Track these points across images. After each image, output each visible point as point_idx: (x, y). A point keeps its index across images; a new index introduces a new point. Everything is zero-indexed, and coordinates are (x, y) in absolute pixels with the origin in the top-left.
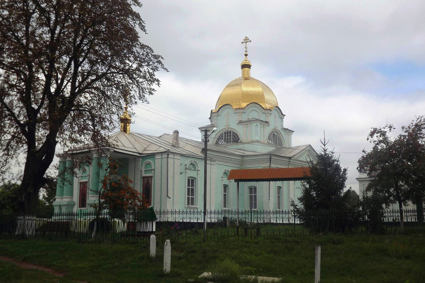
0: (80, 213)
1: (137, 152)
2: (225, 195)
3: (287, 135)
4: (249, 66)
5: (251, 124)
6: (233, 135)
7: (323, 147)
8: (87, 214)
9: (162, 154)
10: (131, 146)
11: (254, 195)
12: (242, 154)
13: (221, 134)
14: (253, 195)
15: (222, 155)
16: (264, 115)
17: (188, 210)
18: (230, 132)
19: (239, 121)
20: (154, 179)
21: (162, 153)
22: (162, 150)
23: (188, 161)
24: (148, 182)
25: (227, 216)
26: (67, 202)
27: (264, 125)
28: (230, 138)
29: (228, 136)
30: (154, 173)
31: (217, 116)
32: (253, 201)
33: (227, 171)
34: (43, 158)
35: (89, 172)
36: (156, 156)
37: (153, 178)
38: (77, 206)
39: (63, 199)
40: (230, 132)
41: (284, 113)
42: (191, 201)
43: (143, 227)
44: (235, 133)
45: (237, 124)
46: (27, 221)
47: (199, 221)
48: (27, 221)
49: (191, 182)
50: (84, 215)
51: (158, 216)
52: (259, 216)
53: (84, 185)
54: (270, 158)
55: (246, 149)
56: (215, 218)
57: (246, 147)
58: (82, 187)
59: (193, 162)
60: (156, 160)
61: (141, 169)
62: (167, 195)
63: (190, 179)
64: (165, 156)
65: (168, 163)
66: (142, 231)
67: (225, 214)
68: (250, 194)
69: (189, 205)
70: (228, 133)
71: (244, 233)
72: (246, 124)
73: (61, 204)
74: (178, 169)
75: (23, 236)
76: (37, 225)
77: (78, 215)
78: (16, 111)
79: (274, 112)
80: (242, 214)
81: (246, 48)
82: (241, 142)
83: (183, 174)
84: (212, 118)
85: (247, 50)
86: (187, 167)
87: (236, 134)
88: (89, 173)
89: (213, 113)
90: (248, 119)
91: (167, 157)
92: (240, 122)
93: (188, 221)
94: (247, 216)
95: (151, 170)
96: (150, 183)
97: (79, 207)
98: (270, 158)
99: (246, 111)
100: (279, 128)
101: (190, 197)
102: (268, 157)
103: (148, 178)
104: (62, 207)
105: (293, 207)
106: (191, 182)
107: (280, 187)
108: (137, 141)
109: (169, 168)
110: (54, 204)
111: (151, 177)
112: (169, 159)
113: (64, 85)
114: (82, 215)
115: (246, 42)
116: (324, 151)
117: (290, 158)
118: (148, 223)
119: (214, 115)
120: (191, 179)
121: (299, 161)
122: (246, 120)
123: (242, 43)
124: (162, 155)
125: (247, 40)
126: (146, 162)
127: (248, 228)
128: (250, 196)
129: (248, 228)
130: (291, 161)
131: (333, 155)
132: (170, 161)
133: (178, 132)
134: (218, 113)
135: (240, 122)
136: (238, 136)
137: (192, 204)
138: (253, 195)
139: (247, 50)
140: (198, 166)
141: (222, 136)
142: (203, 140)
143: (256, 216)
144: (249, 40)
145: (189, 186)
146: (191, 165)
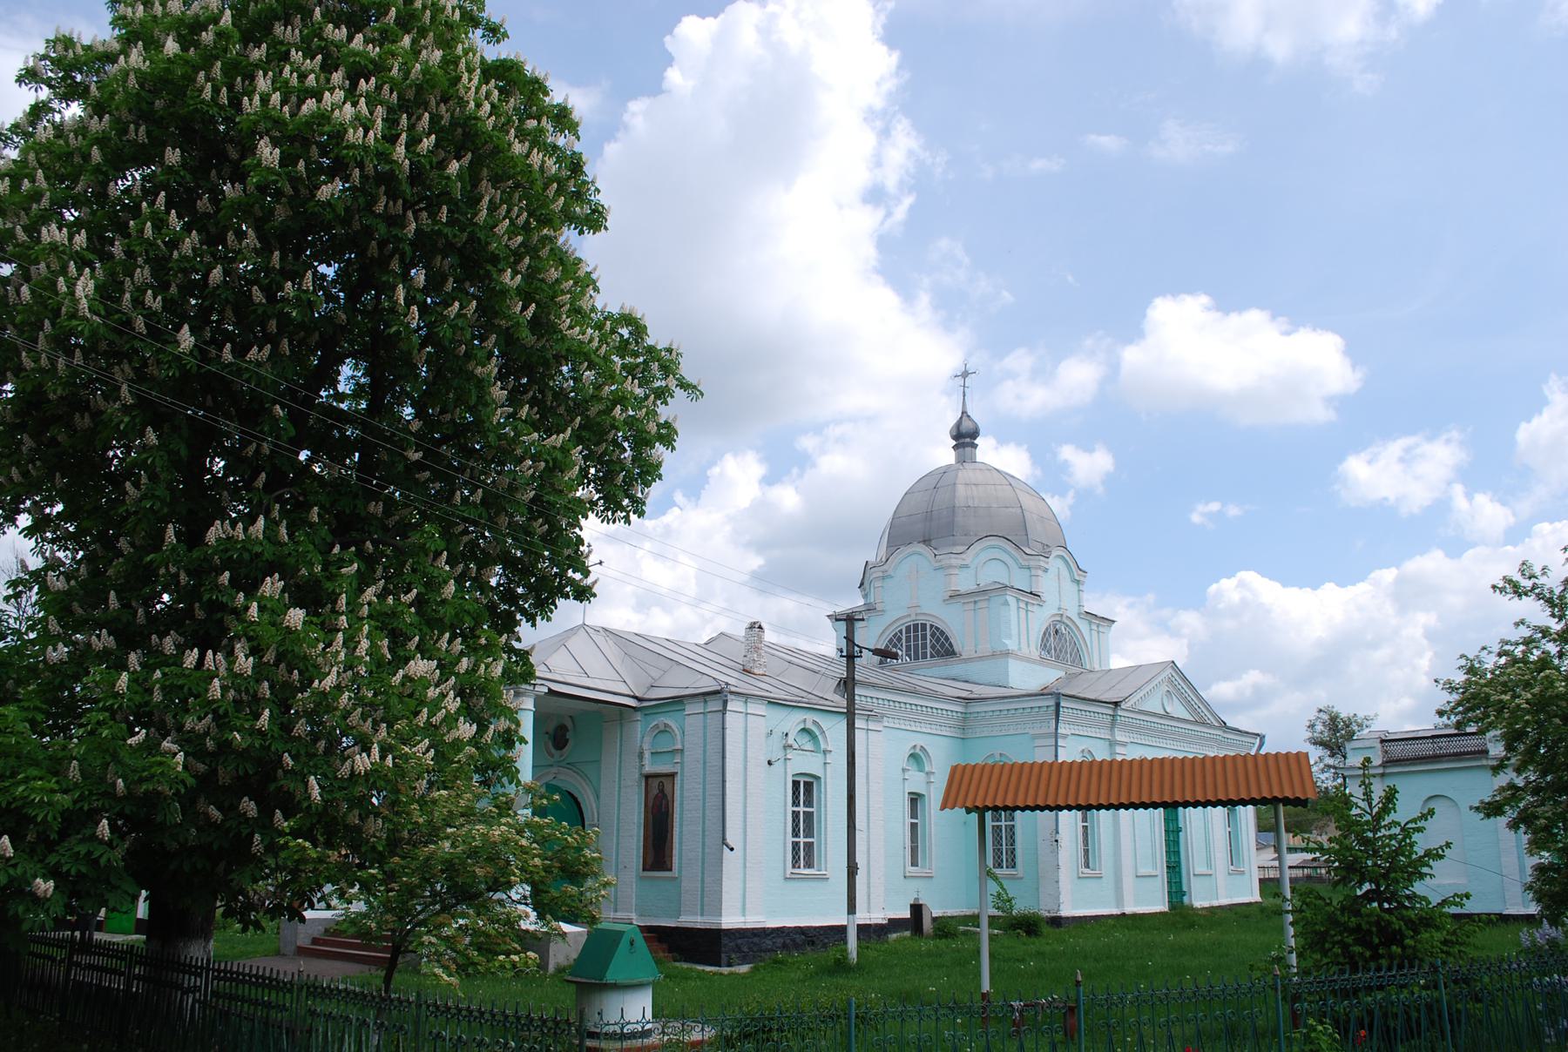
2: (914, 826)
3: (1095, 634)
6: (933, 635)
12: (964, 694)
18: (924, 626)
19: (949, 593)
20: (682, 780)
24: (662, 791)
28: (924, 645)
30: (682, 763)
33: (918, 751)
37: (678, 780)
40: (924, 626)
44: (937, 628)
49: (804, 789)
54: (1058, 705)
55: (974, 678)
59: (809, 725)
62: (724, 839)
64: (714, 705)
69: (799, 867)
70: (916, 630)
74: (760, 751)
83: (778, 766)
87: (942, 633)
92: (955, 596)
96: (669, 798)
100: (1072, 613)
102: (1052, 702)
106: (804, 789)
111: (672, 775)
117: (1116, 704)
120: (802, 780)
122: (973, 587)
124: (705, 702)
125: (965, 374)
128: (993, 826)
130: (1120, 713)
133: (760, 627)
136: (947, 639)
138: (802, 840)
145: (798, 805)
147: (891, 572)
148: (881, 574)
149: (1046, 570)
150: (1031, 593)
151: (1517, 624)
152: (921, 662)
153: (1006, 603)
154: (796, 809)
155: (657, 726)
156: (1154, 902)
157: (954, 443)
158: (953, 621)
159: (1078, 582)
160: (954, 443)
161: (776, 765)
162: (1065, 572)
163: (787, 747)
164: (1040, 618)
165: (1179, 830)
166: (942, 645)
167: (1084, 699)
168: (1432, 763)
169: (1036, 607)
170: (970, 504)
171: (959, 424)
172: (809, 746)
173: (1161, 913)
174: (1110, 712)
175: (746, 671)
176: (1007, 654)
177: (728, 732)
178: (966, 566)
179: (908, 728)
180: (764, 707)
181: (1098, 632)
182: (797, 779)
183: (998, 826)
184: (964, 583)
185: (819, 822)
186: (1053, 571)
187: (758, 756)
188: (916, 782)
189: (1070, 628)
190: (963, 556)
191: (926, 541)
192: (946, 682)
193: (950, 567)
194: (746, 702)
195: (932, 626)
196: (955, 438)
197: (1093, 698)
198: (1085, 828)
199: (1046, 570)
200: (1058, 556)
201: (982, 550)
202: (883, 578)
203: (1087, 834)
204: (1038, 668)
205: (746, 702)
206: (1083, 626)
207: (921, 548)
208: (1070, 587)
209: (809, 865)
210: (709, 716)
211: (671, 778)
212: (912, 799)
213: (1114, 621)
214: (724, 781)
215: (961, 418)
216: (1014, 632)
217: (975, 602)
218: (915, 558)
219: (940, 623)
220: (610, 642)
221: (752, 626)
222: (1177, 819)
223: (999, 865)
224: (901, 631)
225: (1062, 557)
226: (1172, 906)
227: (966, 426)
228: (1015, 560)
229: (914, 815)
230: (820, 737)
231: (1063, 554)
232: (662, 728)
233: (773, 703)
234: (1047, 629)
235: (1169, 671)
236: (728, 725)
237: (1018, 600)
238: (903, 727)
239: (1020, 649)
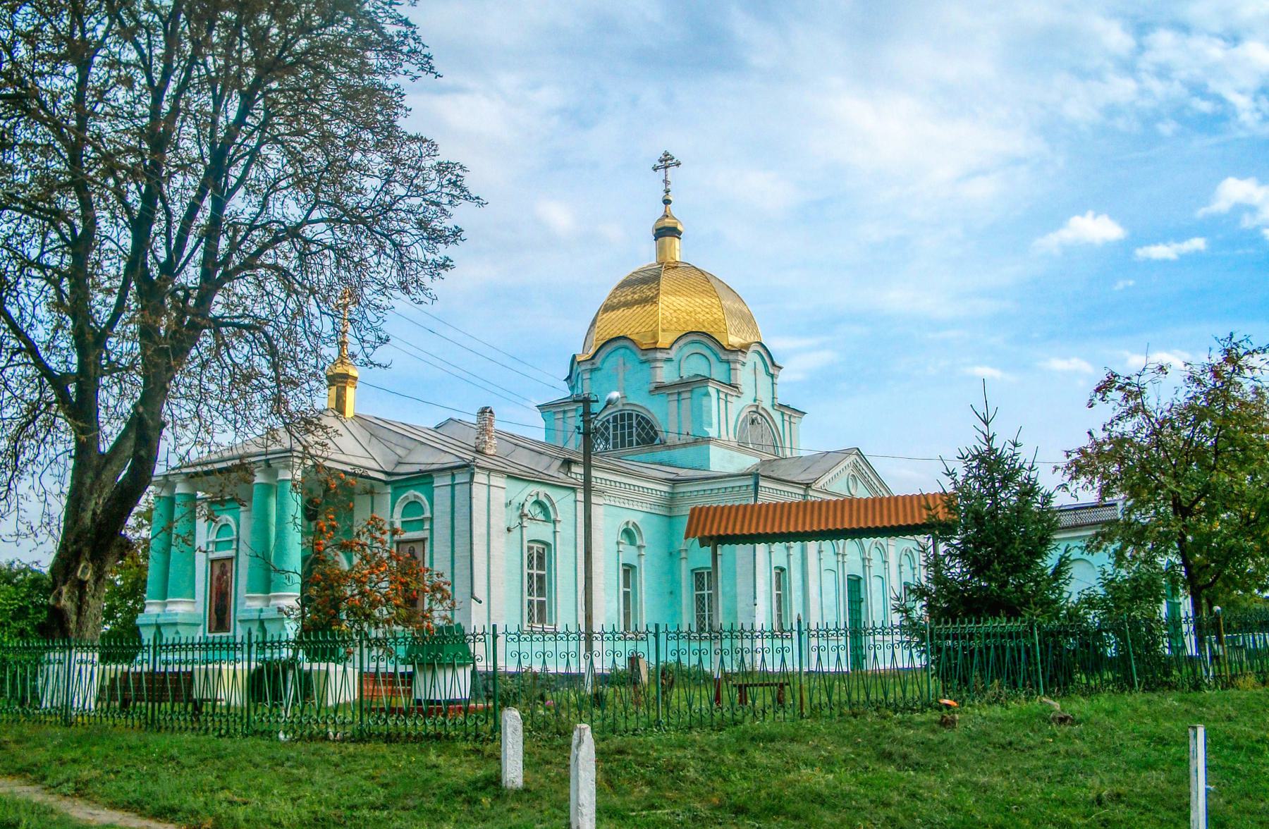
0: (246, 641)
1: (377, 467)
2: (626, 595)
4: (673, 232)
5: (691, 391)
6: (639, 424)
7: (983, 427)
9: (455, 472)
10: (361, 452)
12: (671, 477)
15: (618, 479)
18: (630, 416)
19: (654, 385)
20: (432, 545)
21: (452, 470)
22: (449, 460)
28: (630, 435)
29: (623, 427)
30: (431, 530)
31: (592, 371)
33: (630, 526)
35: (238, 526)
36: (435, 480)
38: (204, 629)
39: (165, 605)
40: (630, 416)
41: (777, 363)
42: (539, 611)
44: (643, 418)
45: (650, 392)
46: (78, 667)
48: (78, 667)
51: (479, 649)
53: (223, 566)
54: (756, 484)
55: (679, 463)
57: (678, 454)
58: (217, 572)
59: (542, 498)
60: (436, 491)
61: (392, 516)
62: (472, 593)
63: (532, 548)
64: (461, 478)
66: (458, 697)
70: (623, 419)
73: (161, 620)
74: (501, 519)
75: (64, 715)
77: (239, 646)
78: (40, 334)
79: (751, 358)
80: (772, 638)
81: (666, 182)
82: (663, 443)
83: (516, 532)
85: (669, 187)
86: (526, 511)
87: (648, 422)
88: (238, 532)
89: (579, 363)
92: (659, 388)
94: (787, 643)
95: (422, 521)
97: (210, 631)
100: (767, 404)
101: (535, 598)
102: (751, 482)
103: (412, 545)
105: (900, 614)
107: (782, 570)
108: (376, 437)
110: (141, 619)
111: (423, 540)
113: (186, 253)
114: (255, 646)
115: (666, 167)
116: (984, 441)
117: (808, 486)
118: (440, 674)
119: (579, 370)
122: (677, 379)
123: (655, 170)
125: (667, 161)
126: (406, 498)
130: (811, 493)
131: (1017, 450)
132: (479, 492)
133: (491, 412)
134: (593, 364)
136: (652, 427)
137: (542, 620)
138: (706, 592)
139: (669, 187)
140: (554, 509)
141: (607, 428)
142: (579, 428)
144: (674, 161)
145: (532, 568)
146: (537, 507)
149: (744, 364)
150: (730, 385)
151: (445, 265)
152: (627, 450)
153: (707, 394)
154: (531, 571)
158: (662, 412)
159: (772, 376)
162: (760, 366)
163: (522, 516)
164: (739, 407)
165: (861, 601)
166: (648, 434)
168: (1075, 531)
169: (735, 398)
172: (541, 517)
174: (802, 492)
175: (478, 451)
176: (707, 440)
177: (474, 501)
178: (669, 360)
179: (622, 505)
181: (790, 423)
182: (531, 545)
183: (701, 595)
185: (550, 584)
186: (750, 366)
187: (499, 522)
188: (629, 554)
192: (653, 466)
193: (656, 360)
194: (489, 476)
195: (637, 416)
198: (779, 596)
199: (744, 364)
201: (686, 345)
204: (736, 454)
205: (489, 476)
206: (777, 416)
208: (764, 381)
211: (421, 543)
212: (625, 570)
214: (471, 544)
216: (715, 420)
217: (565, 412)
218: (622, 351)
220: (356, 424)
221: (483, 411)
222: (859, 590)
224: (608, 421)
227: (668, 222)
228: (716, 355)
229: (626, 584)
230: (550, 509)
233: (511, 477)
235: (853, 458)
236: (474, 494)
237: (718, 391)
238: (618, 504)
239: (719, 436)
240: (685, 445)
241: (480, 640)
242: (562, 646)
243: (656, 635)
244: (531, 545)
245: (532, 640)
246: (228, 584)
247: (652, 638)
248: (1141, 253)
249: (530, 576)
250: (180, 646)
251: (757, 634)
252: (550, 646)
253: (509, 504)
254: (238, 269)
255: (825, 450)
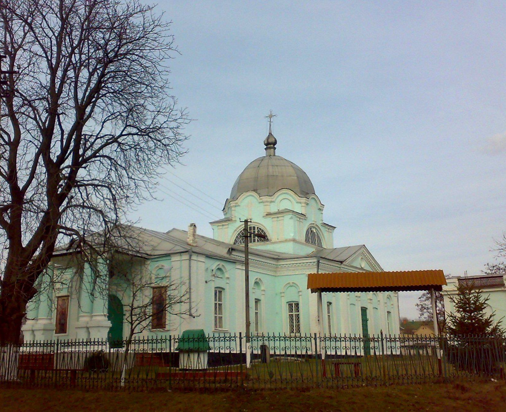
8: (67, 344)
11: (295, 314)
13: (241, 231)
14: (294, 313)
16: (300, 205)
17: (217, 335)
19: (266, 213)
23: (214, 265)
25: (266, 343)
26: (45, 325)
27: (300, 218)
32: (294, 322)
34: (37, 253)
40: (254, 228)
43: (199, 363)
44: (260, 229)
45: (263, 217)
47: (309, 353)
49: (219, 292)
50: (62, 346)
52: (338, 344)
56: (224, 349)
59: (220, 267)
65: (190, 267)
67: (263, 341)
68: (289, 312)
71: (334, 372)
72: (276, 216)
76: (5, 359)
84: (226, 209)
87: (263, 231)
90: (277, 211)
91: (188, 258)
92: (269, 214)
93: (227, 351)
98: (318, 262)
99: (275, 200)
100: (319, 223)
102: (315, 260)
104: (36, 333)
106: (219, 292)
107: (330, 303)
109: (192, 275)
112: (192, 262)
117: (341, 262)
120: (218, 290)
121: (353, 267)
122: (276, 211)
125: (271, 116)
127: (340, 363)
128: (289, 315)
129: (340, 363)
133: (195, 226)
135: (269, 214)
138: (294, 313)
143: (323, 344)
147: (239, 204)
148: (235, 205)
155: (158, 267)
156: (238, 352)
157: (266, 147)
160: (266, 147)
161: (209, 283)
167: (328, 259)
170: (275, 174)
171: (268, 138)
173: (208, 357)
180: (204, 258)
182: (216, 289)
183: (292, 315)
184: (273, 209)
189: (317, 230)
190: (272, 197)
191: (255, 190)
195: (258, 228)
196: (266, 145)
197: (332, 259)
200: (312, 198)
202: (236, 206)
203: (330, 322)
204: (304, 246)
207: (253, 193)
209: (220, 327)
210: (183, 262)
213: (335, 228)
215: (269, 136)
219: (262, 227)
223: (292, 332)
225: (314, 198)
226: (336, 354)
227: (270, 141)
231: (314, 197)
232: (160, 267)
234: (308, 230)
240: (281, 242)
241: (233, 340)
242: (343, 344)
243: (315, 339)
244: (216, 289)
245: (258, 341)
246: (65, 320)
247: (168, 342)
248: (108, 142)
249: (216, 304)
250: (72, 343)
251: (343, 339)
252: (298, 344)
253: (207, 269)
254: (90, 157)
255: (348, 246)
